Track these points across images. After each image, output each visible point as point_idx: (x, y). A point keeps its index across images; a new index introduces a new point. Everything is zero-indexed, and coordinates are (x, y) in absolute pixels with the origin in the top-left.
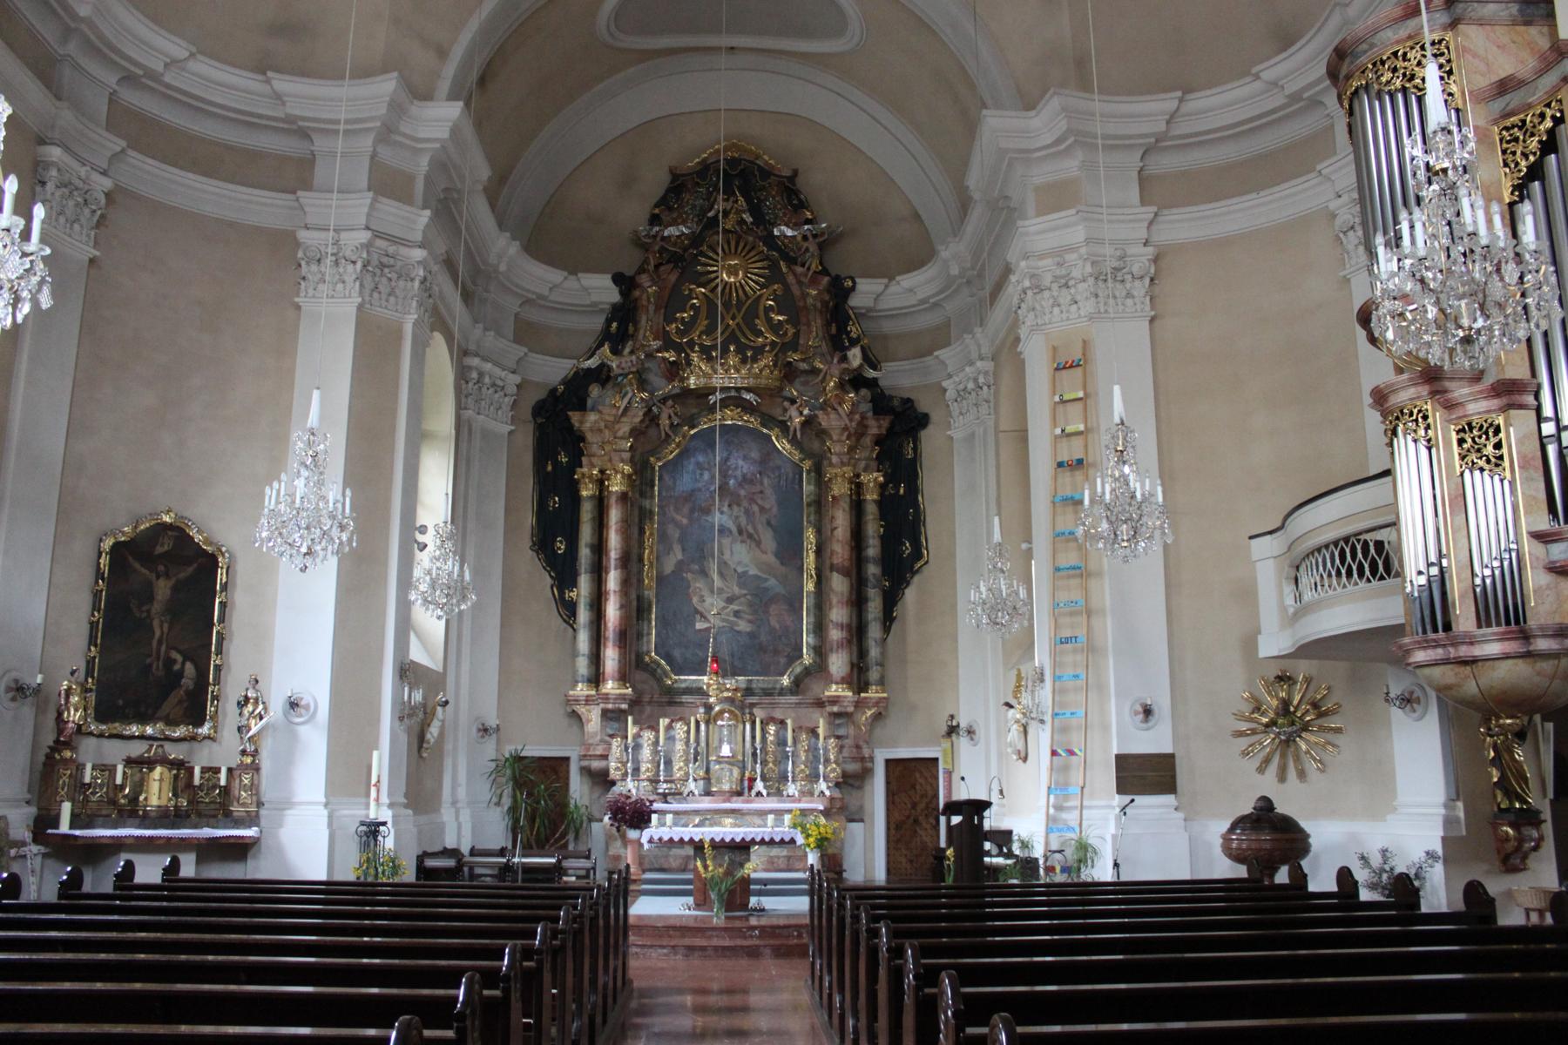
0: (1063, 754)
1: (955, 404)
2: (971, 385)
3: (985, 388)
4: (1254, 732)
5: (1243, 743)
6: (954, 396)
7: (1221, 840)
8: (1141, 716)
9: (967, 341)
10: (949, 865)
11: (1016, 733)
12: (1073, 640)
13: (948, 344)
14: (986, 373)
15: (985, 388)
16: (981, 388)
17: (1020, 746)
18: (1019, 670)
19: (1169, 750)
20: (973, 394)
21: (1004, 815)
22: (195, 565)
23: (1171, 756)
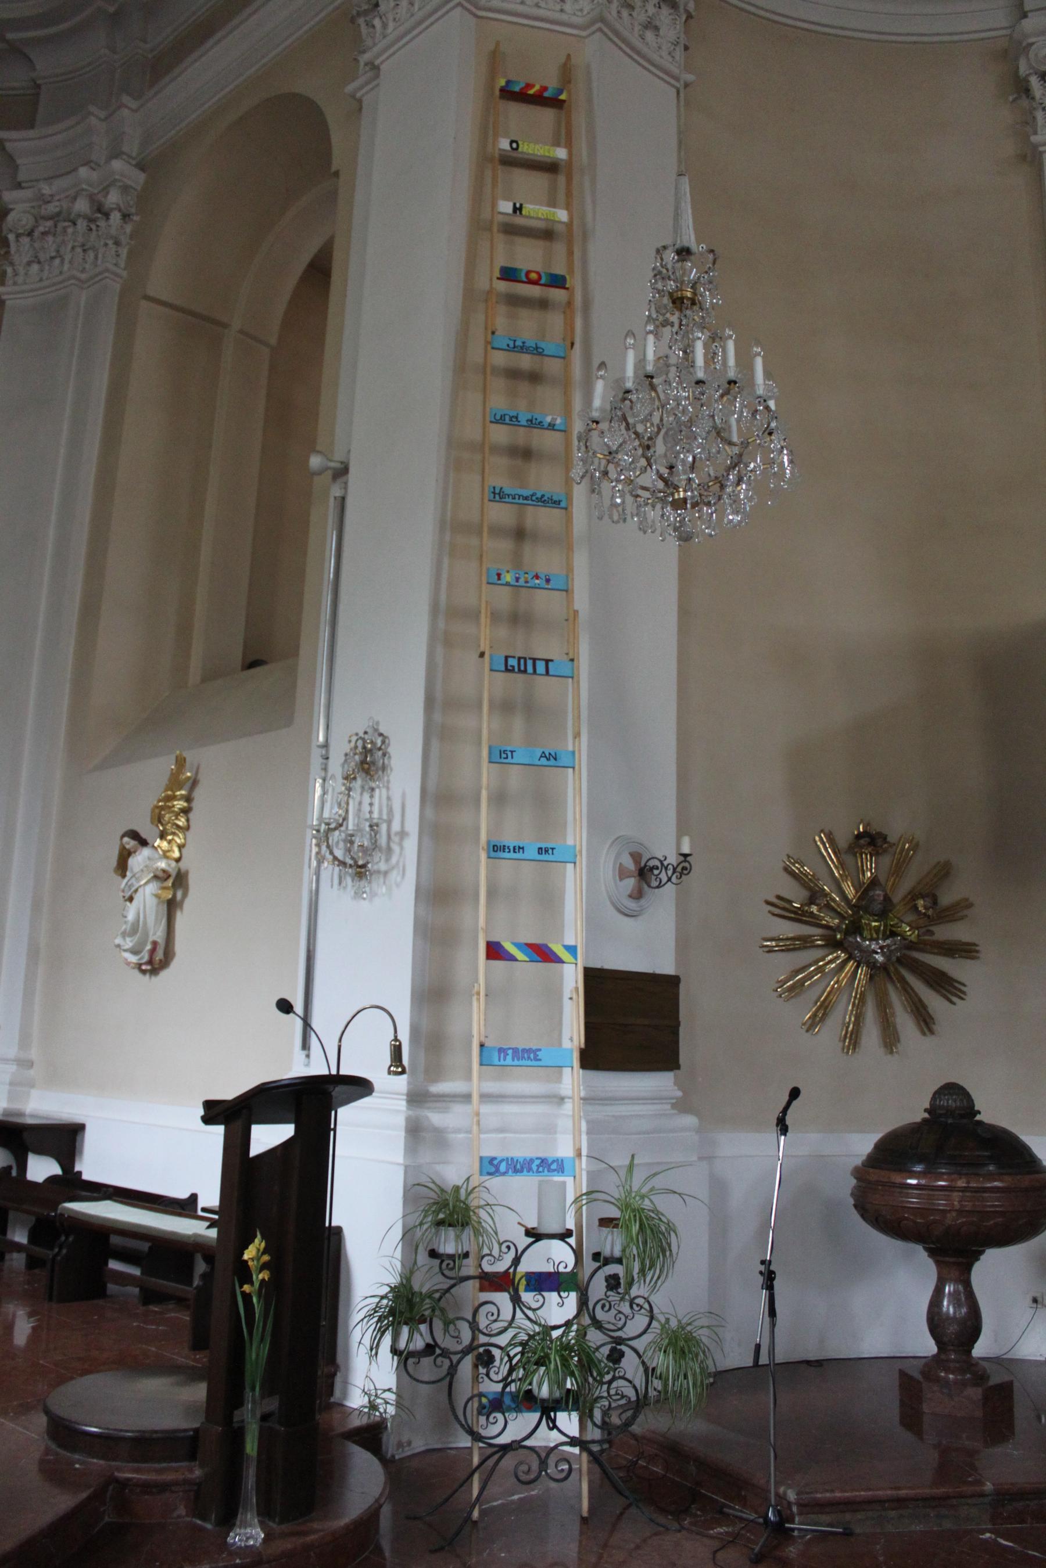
0: (519, 955)
1: (25, 240)
2: (82, 206)
3: (116, 217)
4: (804, 943)
5: (785, 962)
6: (27, 221)
7: (853, 1182)
8: (631, 883)
9: (93, 120)
10: (247, 1297)
11: (151, 903)
12: (541, 667)
13: (30, 124)
14: (125, 189)
15: (116, 217)
16: (107, 215)
17: (158, 934)
18: (181, 762)
19: (667, 968)
20: (82, 224)
21: (32, 1085)
22: (510, 1499)
23: (673, 981)
